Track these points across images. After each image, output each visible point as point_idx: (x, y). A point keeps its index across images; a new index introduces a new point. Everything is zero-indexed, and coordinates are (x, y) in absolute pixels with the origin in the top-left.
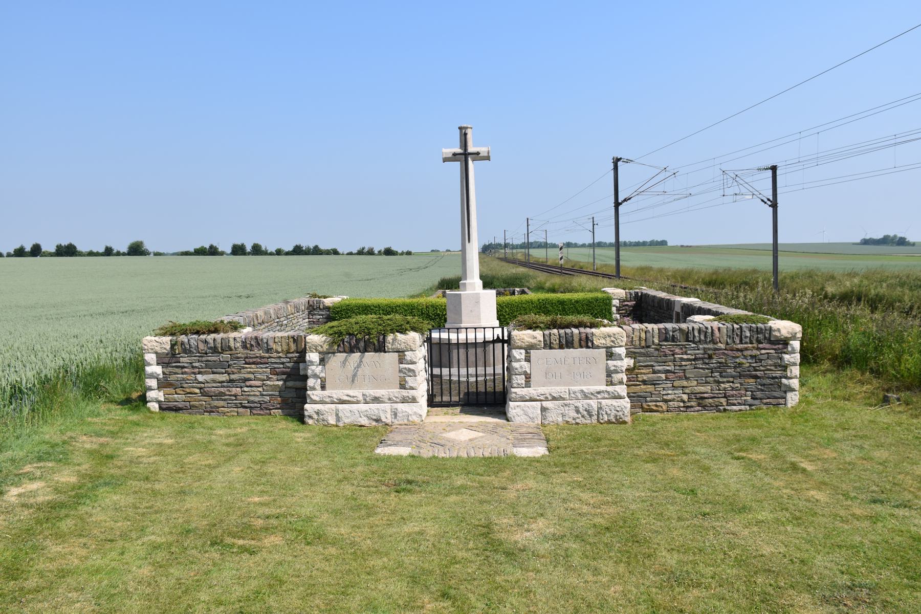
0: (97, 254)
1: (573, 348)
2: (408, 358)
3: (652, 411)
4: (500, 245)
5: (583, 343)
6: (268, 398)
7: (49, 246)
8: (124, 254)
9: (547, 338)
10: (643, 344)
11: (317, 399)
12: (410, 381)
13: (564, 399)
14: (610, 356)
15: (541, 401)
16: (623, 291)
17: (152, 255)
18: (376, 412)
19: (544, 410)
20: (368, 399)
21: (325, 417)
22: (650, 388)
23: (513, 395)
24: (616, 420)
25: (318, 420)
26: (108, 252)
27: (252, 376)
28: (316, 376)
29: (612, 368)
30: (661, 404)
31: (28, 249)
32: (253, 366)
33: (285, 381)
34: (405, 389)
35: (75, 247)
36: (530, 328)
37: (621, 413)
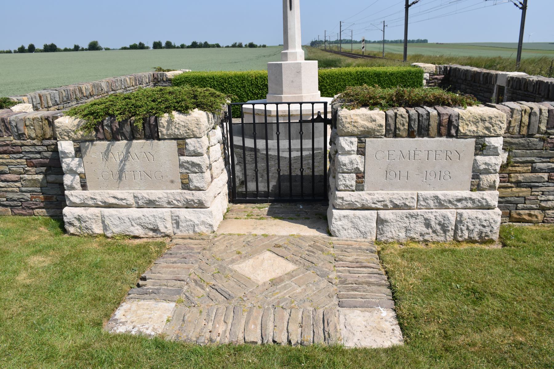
0: (70, 50)
1: (428, 136)
2: (191, 148)
3: (521, 220)
4: (322, 41)
5: (443, 130)
6: (29, 195)
7: (39, 46)
8: (86, 50)
9: (391, 121)
10: (524, 131)
11: (77, 201)
12: (195, 180)
13: (410, 208)
14: (481, 148)
15: (377, 209)
16: (433, 65)
17: (104, 50)
18: (152, 219)
19: (380, 222)
20: (140, 203)
21: (87, 224)
22: (525, 192)
23: (339, 201)
24: (480, 237)
25: (80, 228)
26: (76, 48)
27: (5, 169)
28: (73, 172)
29: (482, 167)
30: (536, 212)
31: (27, 48)
32: (5, 156)
33: (46, 174)
34: (189, 189)
35: (55, 46)
36: (365, 105)
37: (488, 229)
